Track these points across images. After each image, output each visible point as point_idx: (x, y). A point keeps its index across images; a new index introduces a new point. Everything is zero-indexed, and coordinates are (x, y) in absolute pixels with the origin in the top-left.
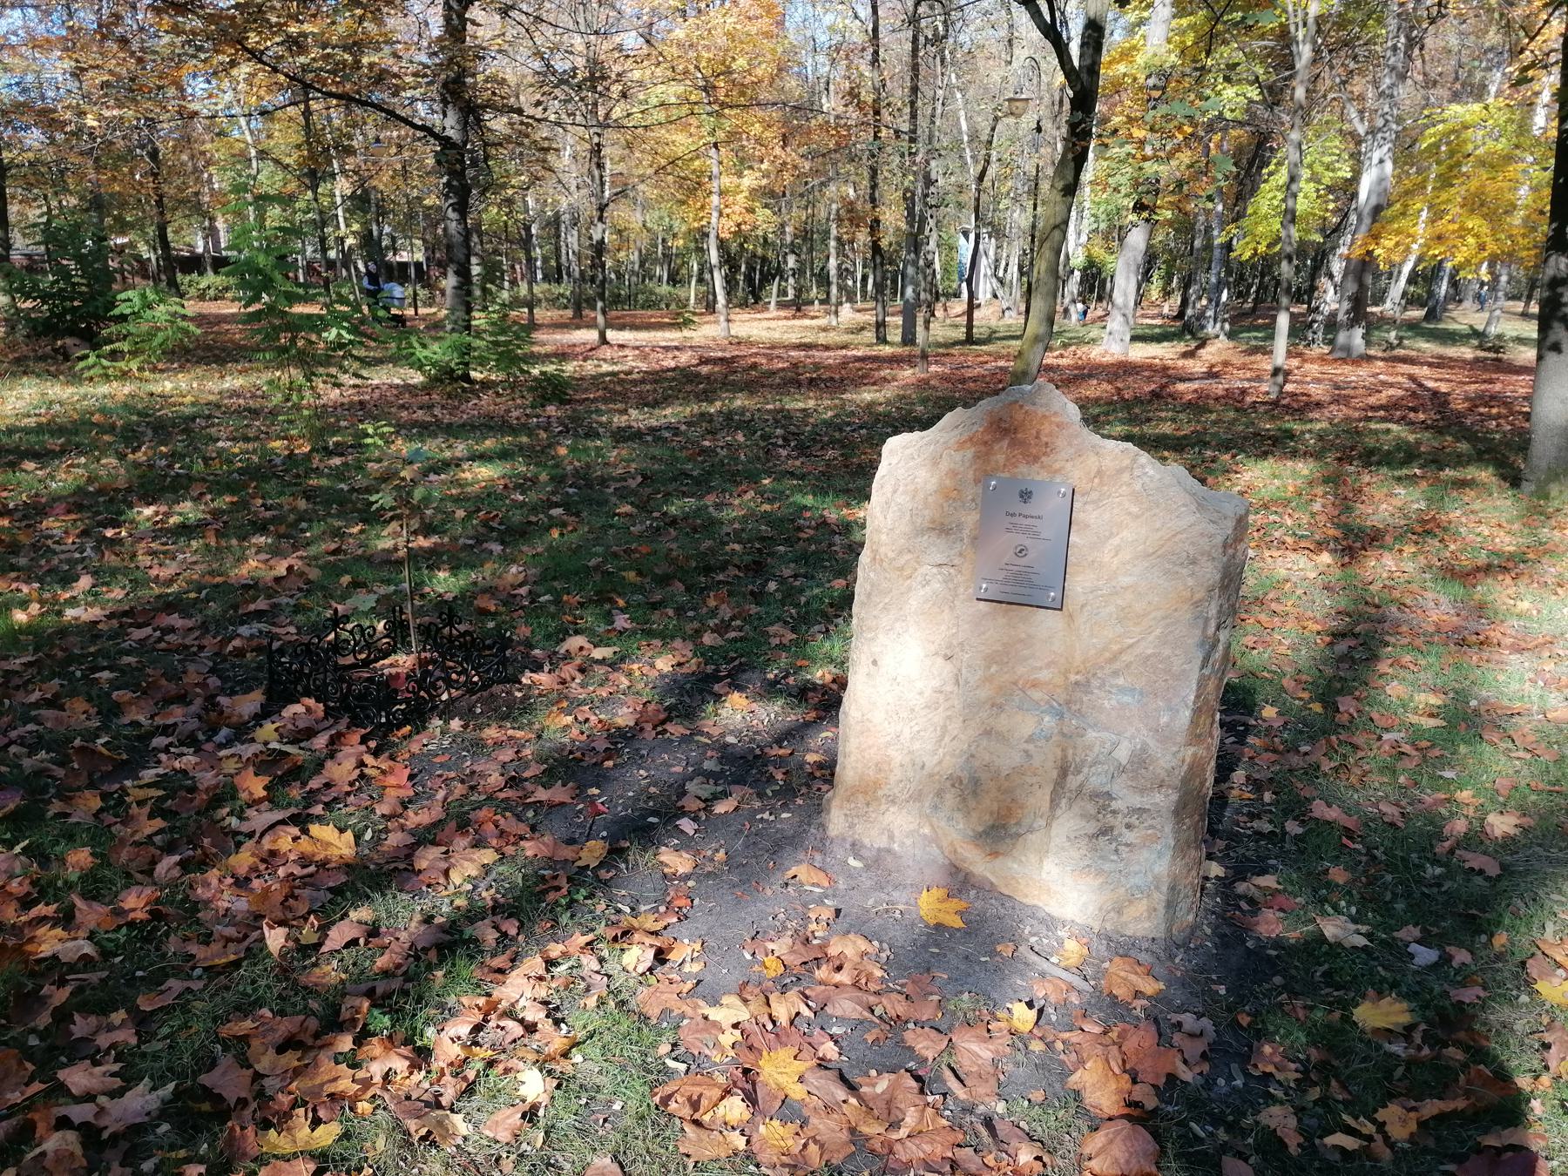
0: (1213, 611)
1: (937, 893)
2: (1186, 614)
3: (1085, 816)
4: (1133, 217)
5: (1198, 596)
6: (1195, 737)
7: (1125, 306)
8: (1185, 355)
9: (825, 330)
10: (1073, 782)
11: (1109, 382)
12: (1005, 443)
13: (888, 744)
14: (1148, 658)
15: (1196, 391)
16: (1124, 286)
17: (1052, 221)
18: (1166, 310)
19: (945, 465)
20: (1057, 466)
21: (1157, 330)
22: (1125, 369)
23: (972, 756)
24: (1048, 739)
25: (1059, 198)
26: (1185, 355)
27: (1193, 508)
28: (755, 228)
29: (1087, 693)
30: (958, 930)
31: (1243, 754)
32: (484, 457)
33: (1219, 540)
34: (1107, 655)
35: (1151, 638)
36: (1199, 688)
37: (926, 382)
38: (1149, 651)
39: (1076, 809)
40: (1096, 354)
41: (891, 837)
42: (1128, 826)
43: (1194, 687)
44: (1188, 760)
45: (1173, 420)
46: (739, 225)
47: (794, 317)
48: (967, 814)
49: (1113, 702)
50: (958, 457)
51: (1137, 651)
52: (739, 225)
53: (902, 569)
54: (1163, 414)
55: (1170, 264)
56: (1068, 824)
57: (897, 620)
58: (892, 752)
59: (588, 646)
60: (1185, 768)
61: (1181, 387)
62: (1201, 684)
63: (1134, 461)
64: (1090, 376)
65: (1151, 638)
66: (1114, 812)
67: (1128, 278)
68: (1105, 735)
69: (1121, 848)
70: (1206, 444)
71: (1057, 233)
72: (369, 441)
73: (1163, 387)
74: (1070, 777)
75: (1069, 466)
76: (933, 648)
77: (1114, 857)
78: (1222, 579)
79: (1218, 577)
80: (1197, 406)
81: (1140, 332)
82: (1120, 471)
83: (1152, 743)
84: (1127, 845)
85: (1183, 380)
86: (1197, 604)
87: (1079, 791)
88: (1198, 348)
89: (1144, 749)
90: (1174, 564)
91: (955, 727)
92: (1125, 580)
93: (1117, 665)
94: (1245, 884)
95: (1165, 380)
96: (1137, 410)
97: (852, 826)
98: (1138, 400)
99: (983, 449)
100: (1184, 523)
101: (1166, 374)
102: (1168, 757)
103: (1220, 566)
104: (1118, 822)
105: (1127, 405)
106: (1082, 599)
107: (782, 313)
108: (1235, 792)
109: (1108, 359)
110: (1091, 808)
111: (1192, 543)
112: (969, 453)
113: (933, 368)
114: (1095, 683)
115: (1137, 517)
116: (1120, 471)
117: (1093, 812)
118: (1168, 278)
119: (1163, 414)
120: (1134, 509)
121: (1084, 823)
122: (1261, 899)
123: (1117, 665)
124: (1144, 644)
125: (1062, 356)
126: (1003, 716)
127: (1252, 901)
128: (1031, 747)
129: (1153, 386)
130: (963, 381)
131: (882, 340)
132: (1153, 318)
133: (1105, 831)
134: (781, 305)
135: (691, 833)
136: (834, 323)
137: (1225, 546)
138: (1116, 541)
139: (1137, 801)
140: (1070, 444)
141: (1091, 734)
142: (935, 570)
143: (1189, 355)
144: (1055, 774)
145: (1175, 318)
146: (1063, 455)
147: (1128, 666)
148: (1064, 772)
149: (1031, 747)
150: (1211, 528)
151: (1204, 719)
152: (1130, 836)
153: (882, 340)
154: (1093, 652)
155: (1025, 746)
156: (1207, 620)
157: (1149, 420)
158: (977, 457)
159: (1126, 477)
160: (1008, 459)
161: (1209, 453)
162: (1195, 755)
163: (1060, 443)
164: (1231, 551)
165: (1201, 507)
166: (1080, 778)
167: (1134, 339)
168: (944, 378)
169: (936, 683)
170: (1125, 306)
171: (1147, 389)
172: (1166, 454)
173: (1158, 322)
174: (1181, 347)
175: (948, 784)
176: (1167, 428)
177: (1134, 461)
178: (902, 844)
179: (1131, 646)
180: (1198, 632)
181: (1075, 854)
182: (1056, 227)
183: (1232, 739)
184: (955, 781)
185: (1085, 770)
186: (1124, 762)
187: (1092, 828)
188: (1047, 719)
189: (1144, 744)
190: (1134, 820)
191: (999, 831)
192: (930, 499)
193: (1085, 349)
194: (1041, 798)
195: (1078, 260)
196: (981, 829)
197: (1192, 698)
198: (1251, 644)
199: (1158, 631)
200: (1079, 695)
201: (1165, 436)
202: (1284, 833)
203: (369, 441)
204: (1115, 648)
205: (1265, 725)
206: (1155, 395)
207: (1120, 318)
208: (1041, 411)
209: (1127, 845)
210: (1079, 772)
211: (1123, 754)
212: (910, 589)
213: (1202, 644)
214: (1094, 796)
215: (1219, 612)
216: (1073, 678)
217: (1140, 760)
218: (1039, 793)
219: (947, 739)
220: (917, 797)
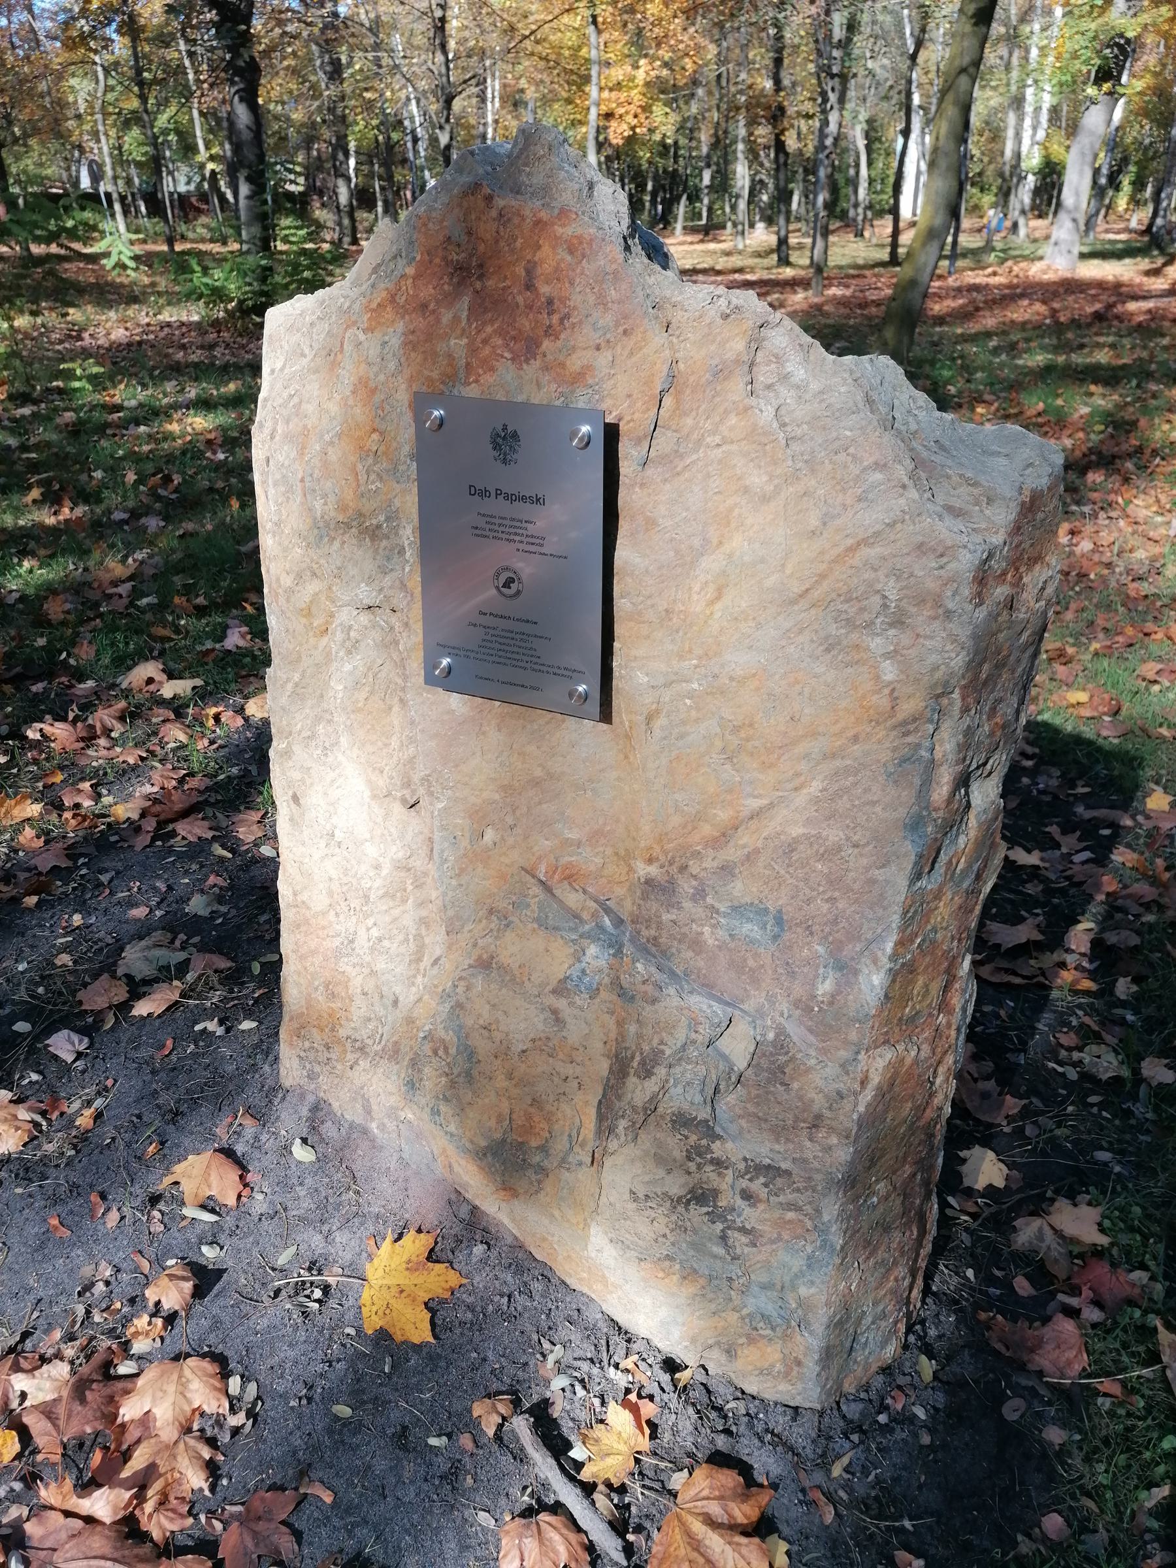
0: (947, 744)
1: (415, 1245)
2: (881, 747)
3: (660, 1159)
4: (1091, 91)
5: (908, 708)
6: (897, 1015)
7: (1077, 208)
8: (1148, 273)
9: (728, 254)
10: (639, 1091)
11: (1044, 302)
12: (464, 304)
13: (338, 954)
14: (791, 847)
15: (1149, 311)
16: (1076, 188)
17: (957, 63)
18: (1133, 224)
19: (348, 374)
20: (575, 363)
21: (1120, 246)
22: (1071, 286)
23: (459, 1006)
24: (594, 993)
25: (968, 28)
26: (1148, 273)
27: (901, 472)
28: (651, 131)
29: (670, 906)
30: (417, 1348)
31: (1098, 886)
32: (205, 404)
33: (966, 562)
34: (707, 830)
35: (801, 799)
36: (908, 918)
37: (818, 308)
38: (797, 831)
39: (646, 1139)
40: (1035, 271)
41: (368, 1111)
42: (747, 1195)
43: (896, 920)
44: (875, 1079)
45: (1113, 346)
46: (633, 128)
47: (702, 241)
48: (461, 1110)
49: (721, 933)
50: (372, 346)
51: (771, 826)
52: (633, 128)
53: (307, 612)
54: (1101, 339)
55: (1142, 166)
56: (624, 1172)
57: (318, 719)
58: (345, 966)
59: (160, 677)
60: (868, 1095)
61: (1132, 306)
62: (916, 912)
63: (756, 344)
64: (1022, 296)
65: (801, 799)
66: (718, 1163)
67: (1081, 173)
68: (698, 1003)
69: (733, 1235)
70: (1149, 376)
71: (964, 80)
72: (77, 384)
73: (1110, 306)
74: (632, 1080)
75: (603, 360)
76: (382, 782)
77: (719, 1250)
78: (974, 666)
79: (958, 661)
80: (1148, 329)
81: (1099, 247)
82: (720, 373)
83: (796, 1031)
84: (743, 1230)
85: (1136, 298)
86: (905, 727)
87: (651, 1109)
88: (1165, 265)
89: (781, 1043)
90: (850, 623)
91: (436, 941)
92: (739, 661)
93: (731, 854)
94: (1037, 1223)
95: (1113, 299)
96: (1070, 335)
97: (312, 1076)
98: (1075, 323)
99: (420, 322)
100: (873, 517)
101: (1118, 291)
102: (831, 1070)
103: (964, 633)
104: (726, 1185)
105: (1058, 328)
106: (648, 699)
107: (689, 239)
108: (1067, 976)
109: (1049, 277)
110: (675, 1146)
111: (897, 574)
112: (395, 334)
113: (834, 291)
114: (686, 886)
115: (765, 499)
116: (720, 373)
117: (678, 1154)
118: (1139, 184)
119: (1101, 339)
120: (757, 480)
121: (661, 1173)
122: (1060, 1270)
123: (731, 854)
124: (782, 813)
125: (995, 274)
126: (509, 936)
127: (1040, 1272)
128: (561, 1004)
129: (1098, 306)
130: (864, 305)
131: (784, 261)
132: (1118, 233)
133: (700, 1196)
134: (688, 230)
135: (69, 1058)
136: (741, 246)
137: (982, 578)
138: (711, 564)
139: (763, 1149)
140: (602, 302)
141: (671, 998)
142: (364, 618)
143: (1155, 272)
144: (604, 1067)
145: (1143, 233)
146: (586, 335)
147: (750, 858)
148: (620, 1068)
149: (561, 1004)
150: (946, 530)
151: (927, 986)
152: (750, 1215)
153: (784, 261)
154: (676, 820)
155: (552, 1000)
156: (931, 765)
157: (1082, 346)
158: (411, 344)
159: (736, 387)
160: (473, 350)
161: (1153, 387)
162: (895, 1067)
163: (580, 298)
164: (1001, 592)
165: (924, 470)
166: (652, 1086)
167: (1083, 256)
168: (841, 302)
169: (396, 852)
170: (1077, 208)
171: (1089, 310)
172: (1093, 388)
173: (1123, 237)
174: (1145, 264)
175: (427, 1049)
176: (1102, 357)
177: (756, 344)
178: (382, 1127)
179: (755, 815)
180: (907, 795)
181: (646, 1231)
182: (963, 70)
183: (1087, 855)
184: (438, 1047)
185: (661, 1071)
186: (741, 1064)
187: (676, 1186)
188: (593, 950)
189: (781, 1032)
190: (757, 1186)
191: (515, 1157)
192: (334, 455)
193: (1023, 265)
194: (580, 1113)
195: (1033, 160)
196: (484, 1143)
197: (889, 947)
198: (1151, 675)
199: (815, 787)
200: (654, 906)
201: (1097, 367)
202: (1138, 1078)
203: (77, 384)
204: (723, 815)
205: (1147, 825)
206: (1098, 317)
207: (1069, 224)
208: (531, 208)
209: (743, 1230)
210: (649, 1074)
211: (737, 1048)
212: (328, 657)
213: (915, 825)
214: (681, 1121)
215: (964, 747)
216: (644, 870)
217: (774, 1065)
218: (579, 1098)
219: (427, 961)
220: (394, 1053)
